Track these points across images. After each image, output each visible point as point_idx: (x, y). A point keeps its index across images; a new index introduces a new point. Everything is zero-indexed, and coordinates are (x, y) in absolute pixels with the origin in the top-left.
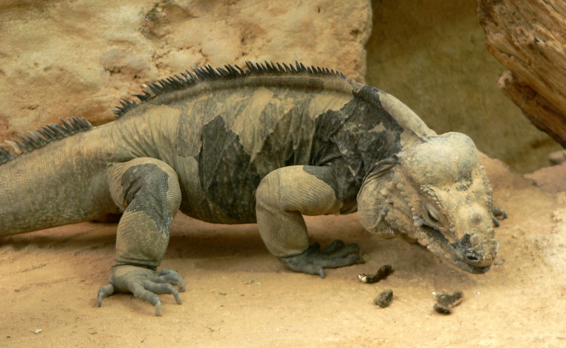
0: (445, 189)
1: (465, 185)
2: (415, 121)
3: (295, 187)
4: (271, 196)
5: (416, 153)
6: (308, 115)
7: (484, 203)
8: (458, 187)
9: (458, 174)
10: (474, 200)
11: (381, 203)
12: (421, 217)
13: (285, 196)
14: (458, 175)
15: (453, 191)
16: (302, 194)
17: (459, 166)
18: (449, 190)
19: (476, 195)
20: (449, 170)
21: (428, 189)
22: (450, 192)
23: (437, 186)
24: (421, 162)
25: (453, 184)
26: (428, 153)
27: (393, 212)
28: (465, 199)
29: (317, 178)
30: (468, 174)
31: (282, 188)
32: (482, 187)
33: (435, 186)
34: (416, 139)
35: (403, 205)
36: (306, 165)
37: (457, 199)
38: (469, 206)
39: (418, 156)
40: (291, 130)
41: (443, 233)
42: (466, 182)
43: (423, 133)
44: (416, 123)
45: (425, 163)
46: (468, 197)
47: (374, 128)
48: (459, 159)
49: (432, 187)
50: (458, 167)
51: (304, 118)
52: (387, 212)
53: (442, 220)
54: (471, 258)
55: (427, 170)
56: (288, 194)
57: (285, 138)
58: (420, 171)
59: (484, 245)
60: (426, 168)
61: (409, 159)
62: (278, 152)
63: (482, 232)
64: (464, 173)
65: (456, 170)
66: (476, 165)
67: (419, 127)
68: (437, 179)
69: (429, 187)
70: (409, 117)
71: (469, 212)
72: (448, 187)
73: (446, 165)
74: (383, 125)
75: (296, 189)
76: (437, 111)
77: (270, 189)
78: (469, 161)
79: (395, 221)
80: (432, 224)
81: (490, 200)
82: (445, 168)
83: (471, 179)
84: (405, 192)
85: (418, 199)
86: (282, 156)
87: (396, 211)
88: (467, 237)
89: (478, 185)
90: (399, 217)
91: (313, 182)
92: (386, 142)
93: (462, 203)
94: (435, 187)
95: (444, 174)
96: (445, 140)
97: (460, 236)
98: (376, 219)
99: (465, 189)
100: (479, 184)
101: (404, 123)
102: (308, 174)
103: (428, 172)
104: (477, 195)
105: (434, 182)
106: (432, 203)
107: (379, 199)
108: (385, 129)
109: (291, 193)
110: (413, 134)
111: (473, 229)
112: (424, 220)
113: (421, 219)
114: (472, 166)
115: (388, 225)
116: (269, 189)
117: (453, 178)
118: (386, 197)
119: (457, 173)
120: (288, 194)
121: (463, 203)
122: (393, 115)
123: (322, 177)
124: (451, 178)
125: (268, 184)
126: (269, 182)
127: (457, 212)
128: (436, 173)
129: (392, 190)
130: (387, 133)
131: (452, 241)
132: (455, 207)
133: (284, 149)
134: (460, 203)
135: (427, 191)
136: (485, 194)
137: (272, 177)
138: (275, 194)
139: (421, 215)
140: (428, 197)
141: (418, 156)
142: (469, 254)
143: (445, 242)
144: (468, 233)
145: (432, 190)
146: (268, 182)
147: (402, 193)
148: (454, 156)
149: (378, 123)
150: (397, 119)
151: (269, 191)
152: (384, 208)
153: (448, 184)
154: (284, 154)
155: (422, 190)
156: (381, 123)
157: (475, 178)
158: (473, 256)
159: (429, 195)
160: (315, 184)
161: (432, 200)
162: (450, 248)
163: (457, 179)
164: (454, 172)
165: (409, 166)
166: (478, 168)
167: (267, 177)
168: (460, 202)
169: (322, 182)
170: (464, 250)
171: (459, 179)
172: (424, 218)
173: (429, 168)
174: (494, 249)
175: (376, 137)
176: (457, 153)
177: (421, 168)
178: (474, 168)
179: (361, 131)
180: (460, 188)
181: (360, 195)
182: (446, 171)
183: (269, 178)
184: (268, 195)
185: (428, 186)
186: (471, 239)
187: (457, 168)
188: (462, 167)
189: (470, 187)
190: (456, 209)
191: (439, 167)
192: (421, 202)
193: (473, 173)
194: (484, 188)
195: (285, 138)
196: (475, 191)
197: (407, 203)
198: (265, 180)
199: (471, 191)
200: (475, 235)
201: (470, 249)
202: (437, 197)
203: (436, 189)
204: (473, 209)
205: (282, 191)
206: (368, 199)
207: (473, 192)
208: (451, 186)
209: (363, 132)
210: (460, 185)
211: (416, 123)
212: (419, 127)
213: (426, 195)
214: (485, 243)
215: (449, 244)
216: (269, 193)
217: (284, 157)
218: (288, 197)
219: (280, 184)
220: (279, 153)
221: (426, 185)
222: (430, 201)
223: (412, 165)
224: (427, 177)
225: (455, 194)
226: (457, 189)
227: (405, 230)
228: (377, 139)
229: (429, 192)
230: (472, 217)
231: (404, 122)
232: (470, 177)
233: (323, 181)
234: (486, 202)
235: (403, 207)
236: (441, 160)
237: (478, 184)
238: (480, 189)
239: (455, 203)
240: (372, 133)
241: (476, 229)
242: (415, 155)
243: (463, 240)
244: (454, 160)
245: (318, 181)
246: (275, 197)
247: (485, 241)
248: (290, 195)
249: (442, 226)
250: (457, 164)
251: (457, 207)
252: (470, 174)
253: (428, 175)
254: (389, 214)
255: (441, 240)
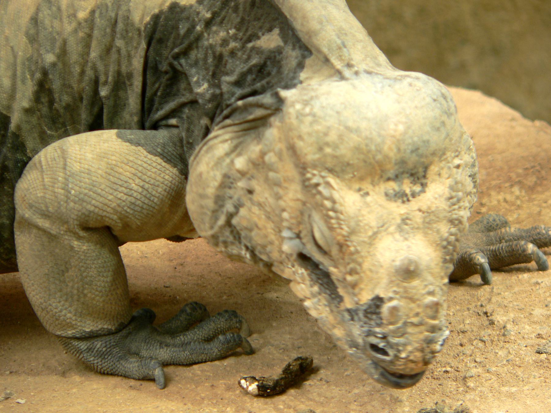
0: (360, 190)
1: (408, 191)
2: (334, 33)
3: (100, 172)
4: (47, 196)
5: (317, 97)
6: (128, 18)
7: (437, 239)
8: (392, 191)
9: (396, 164)
10: (418, 228)
11: (232, 186)
12: (298, 236)
13: (80, 193)
14: (396, 167)
15: (375, 197)
16: (115, 187)
17: (403, 147)
18: (367, 194)
19: (424, 218)
20: (377, 150)
21: (321, 181)
22: (369, 199)
23: (343, 180)
24: (320, 120)
25: (382, 183)
26: (342, 103)
27: (250, 210)
28: (399, 221)
29: (149, 152)
30: (421, 170)
31: (72, 175)
32: (443, 205)
33: (338, 177)
34: (333, 71)
35: (271, 200)
36: (134, 129)
37: (382, 216)
38: (402, 239)
39: (317, 106)
40: (94, 54)
41: (336, 282)
42: (411, 185)
43: (346, 62)
44: (335, 37)
45: (328, 124)
46: (407, 219)
47: (259, 38)
48: (405, 133)
49: (332, 180)
50: (399, 150)
51: (120, 26)
52: (238, 207)
53: (334, 251)
54: (374, 347)
55: (328, 139)
56: (85, 189)
57: (83, 73)
58: (313, 139)
59: (410, 330)
60: (326, 134)
61: (298, 106)
62: (67, 107)
63: (412, 300)
64: (410, 165)
65: (391, 154)
66: (444, 154)
67: (340, 48)
68: (345, 164)
69: (323, 177)
70: (321, 23)
71: (397, 251)
72: (367, 186)
73: (371, 139)
74: (279, 35)
75: (102, 176)
76: (408, 13)
77: (46, 180)
78: (428, 141)
79: (251, 230)
80: (317, 256)
81: (453, 238)
82: (367, 145)
83: (424, 181)
84: (278, 175)
85: (300, 196)
86: (79, 115)
87: (255, 209)
88: (378, 301)
89: (436, 199)
90: (260, 224)
91: (140, 162)
92: (279, 72)
93: (389, 227)
94: (338, 181)
95: (362, 156)
96: (390, 86)
97: (366, 297)
98: (217, 219)
99: (405, 199)
100: (440, 196)
101: (310, 37)
102: (128, 144)
103: (327, 144)
104: (427, 220)
105: (337, 169)
106: (321, 211)
107: (229, 177)
108: (282, 44)
109: (91, 187)
110: (327, 60)
111: (395, 289)
112: (304, 244)
113: (297, 241)
114: (434, 154)
115: (237, 236)
116: (43, 181)
117: (382, 171)
118: (243, 174)
119: (393, 161)
120: (85, 189)
121: (392, 229)
122: (291, 16)
123: (159, 150)
124: (377, 168)
125: (42, 171)
126: (44, 167)
127: (371, 244)
128: (344, 151)
129: (257, 163)
130: (284, 53)
131: (348, 303)
132: (370, 233)
133: (81, 99)
134: (383, 226)
135: (317, 185)
136: (445, 222)
137: (48, 156)
138: (56, 190)
139: (300, 232)
140: (318, 197)
141: (317, 106)
142: (373, 340)
143: (336, 302)
144: (382, 295)
145: (328, 184)
146: (42, 167)
147: (271, 174)
148: (396, 125)
149: (270, 30)
150: (297, 25)
151: (44, 185)
152: (236, 197)
153: (369, 180)
154: (83, 109)
155: (309, 179)
156: (276, 31)
157: (433, 181)
158: (381, 345)
159: (320, 193)
160: (145, 165)
161: (322, 205)
162: (343, 316)
163: (391, 174)
164: (386, 157)
165: (294, 122)
166: (448, 162)
167: (40, 157)
168: (386, 226)
169: (159, 160)
170: (366, 329)
171: (397, 176)
172: (304, 241)
173: (333, 137)
174: (430, 341)
175: (260, 58)
176: (404, 120)
177: (317, 132)
178: (436, 159)
179: (233, 44)
180: (395, 195)
181: (195, 158)
182: (369, 151)
183: (42, 159)
184: (42, 194)
185: (323, 174)
186: (385, 309)
187: (395, 150)
188: (408, 151)
189: (418, 198)
190: (370, 237)
191: (354, 139)
192: (304, 204)
193: (434, 169)
194: (447, 208)
195: (83, 73)
196: (424, 208)
197: (278, 197)
198: (35, 164)
199: (416, 208)
200: (394, 303)
201: (377, 330)
202: (334, 202)
203: (338, 184)
204: (409, 247)
205: (72, 183)
206: (208, 172)
207: (420, 210)
208: (374, 186)
209: (236, 47)
210: (397, 188)
211: (335, 37)
212: (340, 48)
213: (314, 191)
214: (413, 325)
215: (342, 307)
216: (45, 189)
217: (84, 116)
218: (85, 195)
219: (68, 168)
220: (71, 109)
221: (320, 172)
222: (319, 207)
223: (302, 122)
224: (325, 156)
225: (380, 205)
226: (387, 195)
227: (268, 255)
228: (262, 62)
229: (320, 188)
230: (398, 263)
231: (311, 33)
232: (424, 177)
233: (162, 159)
234: (442, 240)
235: (271, 207)
236: (364, 125)
237: (436, 196)
238: (437, 207)
239: (374, 224)
240: (253, 48)
241: (401, 290)
242: (313, 103)
243: (370, 307)
244: (392, 132)
245: (151, 159)
246: (56, 197)
247: (415, 320)
248: (90, 190)
249: (336, 267)
250: (398, 142)
251: (375, 234)
252: (425, 171)
253: (328, 150)
254: (243, 212)
255: (330, 295)
